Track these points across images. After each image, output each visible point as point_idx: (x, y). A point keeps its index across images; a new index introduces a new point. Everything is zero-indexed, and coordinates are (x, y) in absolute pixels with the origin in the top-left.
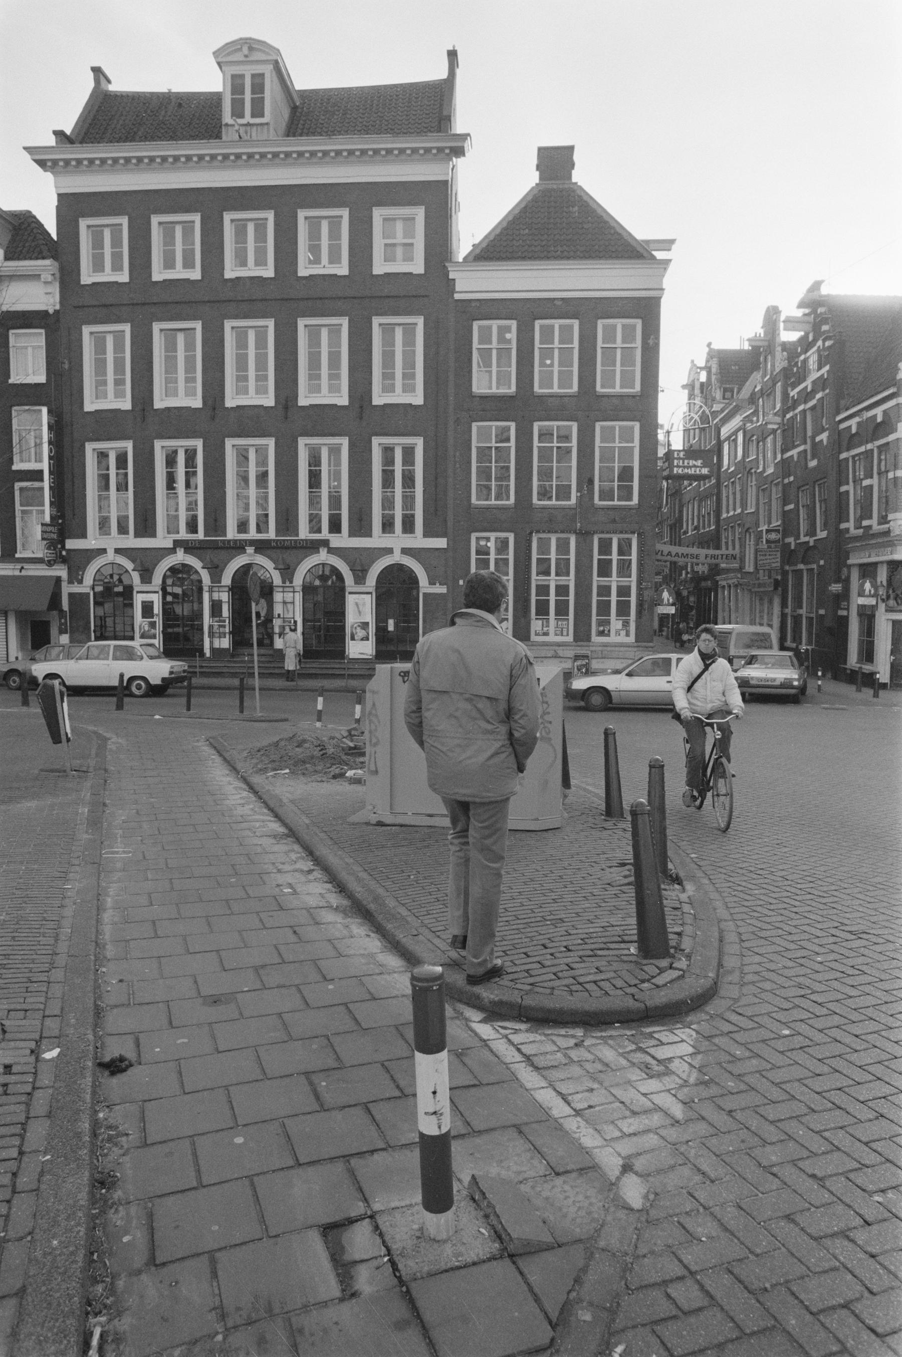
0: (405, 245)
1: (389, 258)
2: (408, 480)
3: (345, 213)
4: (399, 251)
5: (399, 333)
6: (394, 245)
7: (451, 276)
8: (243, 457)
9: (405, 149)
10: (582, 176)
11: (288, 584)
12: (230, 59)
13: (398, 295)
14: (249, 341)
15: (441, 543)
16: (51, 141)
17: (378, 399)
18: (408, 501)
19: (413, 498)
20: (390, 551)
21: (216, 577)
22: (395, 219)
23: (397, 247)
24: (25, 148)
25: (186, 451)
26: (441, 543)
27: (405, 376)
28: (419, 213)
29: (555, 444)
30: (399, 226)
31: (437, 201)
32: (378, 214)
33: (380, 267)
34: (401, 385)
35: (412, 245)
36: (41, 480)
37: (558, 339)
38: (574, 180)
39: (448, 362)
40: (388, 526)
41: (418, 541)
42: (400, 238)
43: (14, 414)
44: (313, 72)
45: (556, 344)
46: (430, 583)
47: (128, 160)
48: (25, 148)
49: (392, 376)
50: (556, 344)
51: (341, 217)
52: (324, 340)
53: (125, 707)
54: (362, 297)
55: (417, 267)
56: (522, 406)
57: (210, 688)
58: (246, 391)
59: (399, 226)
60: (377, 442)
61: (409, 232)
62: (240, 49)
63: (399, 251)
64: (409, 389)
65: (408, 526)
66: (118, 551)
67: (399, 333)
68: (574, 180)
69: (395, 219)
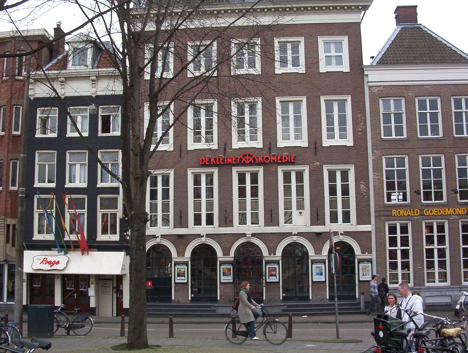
0: (336, 56)
1: (328, 63)
2: (333, 191)
3: (302, 39)
4: (334, 61)
5: (291, 107)
6: (330, 56)
7: (366, 73)
10: (425, 19)
11: (272, 255)
13: (335, 83)
17: (326, 143)
18: (346, 204)
19: (168, 205)
20: (199, 236)
22: (330, 43)
23: (332, 58)
25: (251, 174)
27: (207, 133)
28: (345, 40)
29: (396, 168)
30: (333, 47)
31: (353, 32)
32: (321, 40)
33: (323, 68)
35: (341, 56)
36: (118, 193)
38: (419, 23)
40: (198, 221)
41: (353, 226)
42: (333, 53)
43: (68, 156)
45: (428, 110)
46: (270, 254)
49: (333, 130)
51: (300, 42)
53: (294, 337)
54: (314, 84)
55: (345, 68)
57: (215, 323)
58: (244, 140)
59: (333, 47)
60: (325, 169)
61: (339, 49)
63: (334, 61)
64: (343, 136)
65: (346, 218)
66: (163, 236)
67: (291, 107)
68: (419, 23)
69: (330, 43)
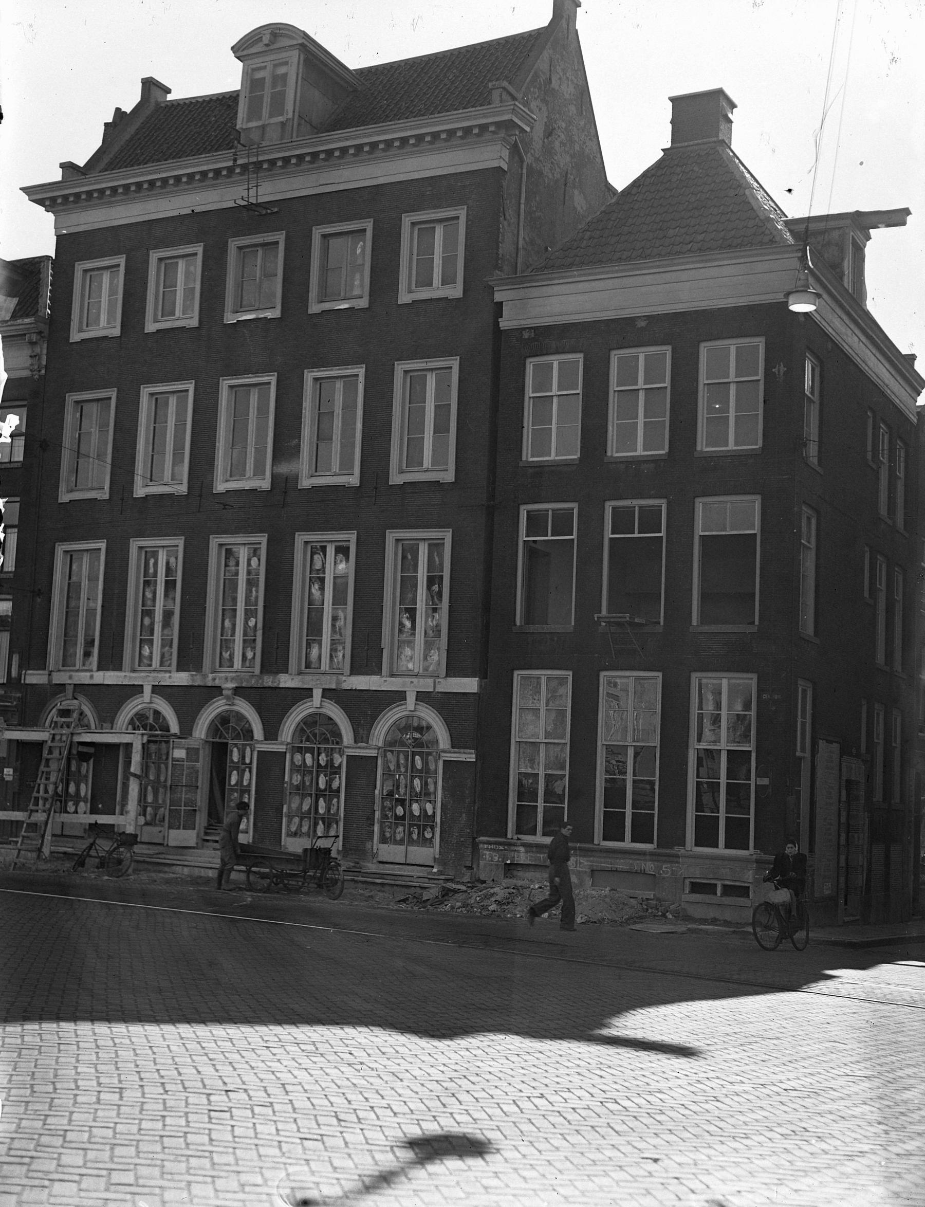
8: (409, 554)
9: (393, 140)
12: (245, 53)
14: (247, 403)
15: (469, 685)
16: (56, 175)
21: (187, 730)
24: (21, 189)
26: (469, 685)
34: (428, 455)
37: (640, 372)
39: (492, 415)
44: (359, 47)
47: (191, 176)
48: (21, 189)
50: (555, 391)
52: (336, 392)
54: (383, 335)
56: (593, 475)
62: (260, 39)
